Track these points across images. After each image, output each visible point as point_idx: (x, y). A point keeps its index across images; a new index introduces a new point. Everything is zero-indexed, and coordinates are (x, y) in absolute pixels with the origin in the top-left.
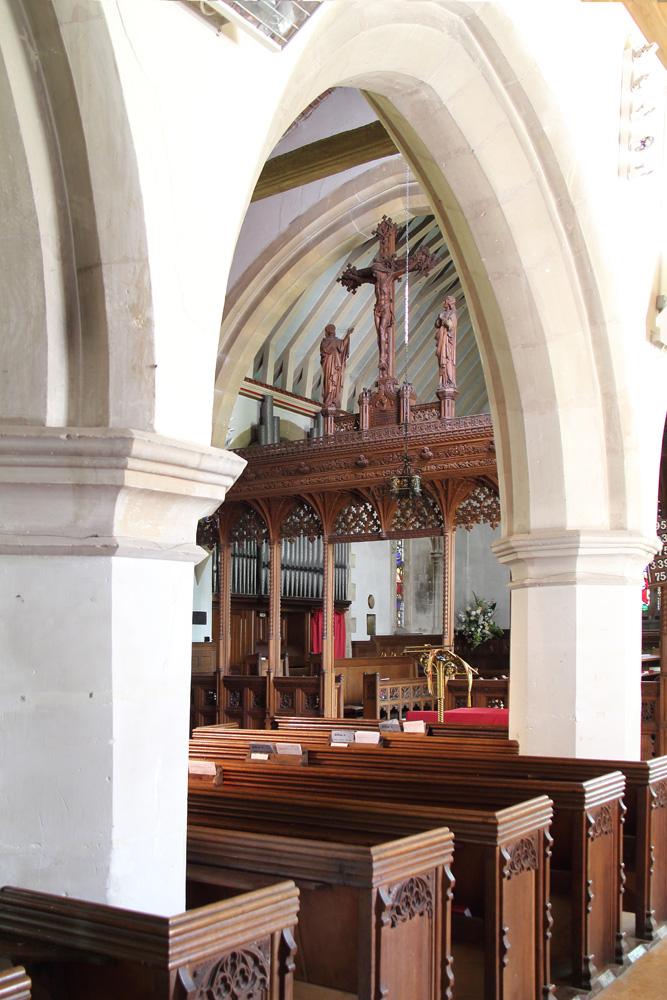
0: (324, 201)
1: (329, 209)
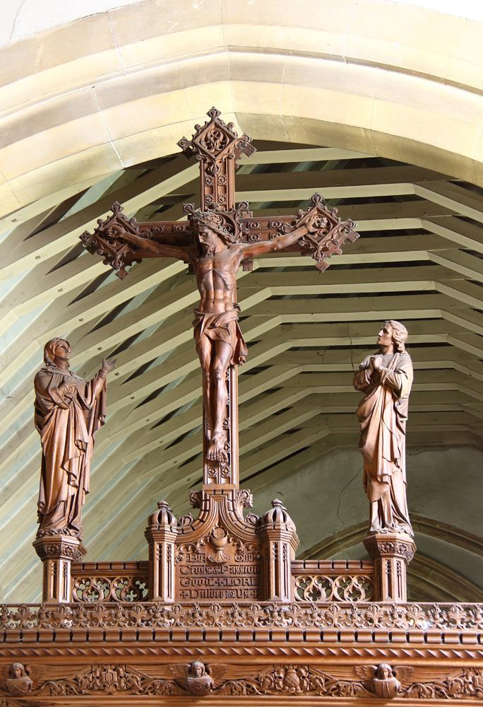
0: (24, 45)
1: (42, 68)
